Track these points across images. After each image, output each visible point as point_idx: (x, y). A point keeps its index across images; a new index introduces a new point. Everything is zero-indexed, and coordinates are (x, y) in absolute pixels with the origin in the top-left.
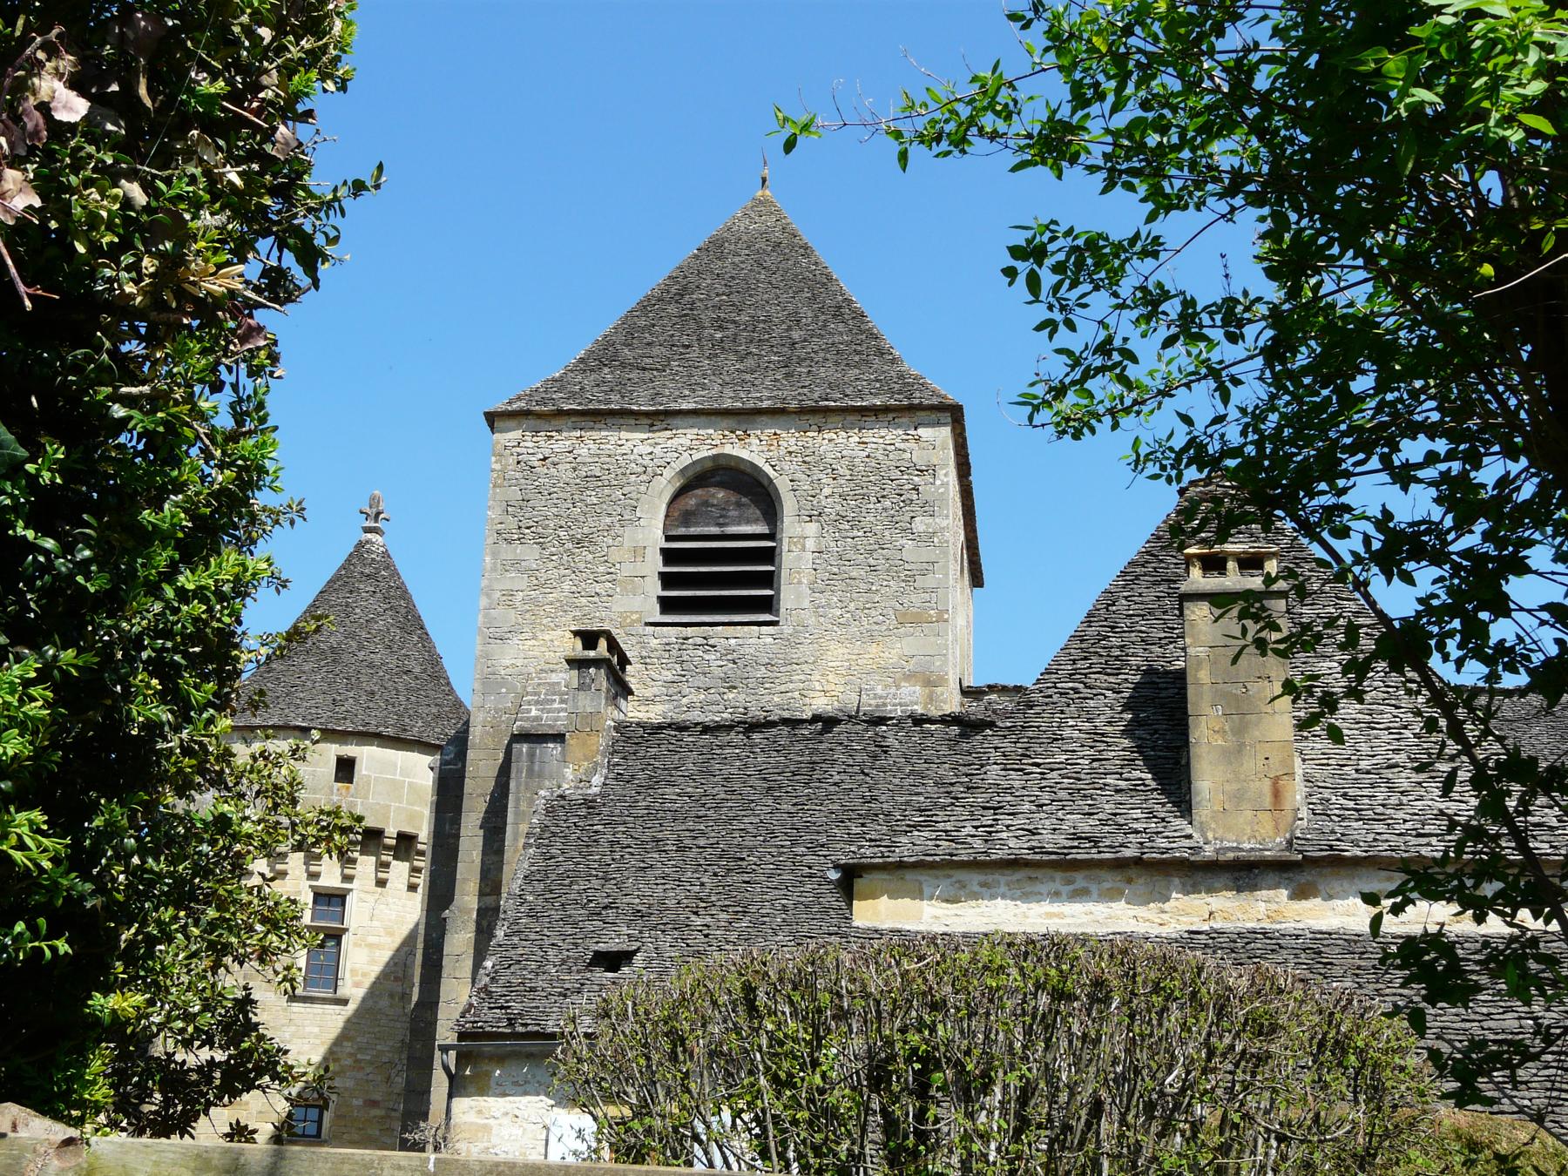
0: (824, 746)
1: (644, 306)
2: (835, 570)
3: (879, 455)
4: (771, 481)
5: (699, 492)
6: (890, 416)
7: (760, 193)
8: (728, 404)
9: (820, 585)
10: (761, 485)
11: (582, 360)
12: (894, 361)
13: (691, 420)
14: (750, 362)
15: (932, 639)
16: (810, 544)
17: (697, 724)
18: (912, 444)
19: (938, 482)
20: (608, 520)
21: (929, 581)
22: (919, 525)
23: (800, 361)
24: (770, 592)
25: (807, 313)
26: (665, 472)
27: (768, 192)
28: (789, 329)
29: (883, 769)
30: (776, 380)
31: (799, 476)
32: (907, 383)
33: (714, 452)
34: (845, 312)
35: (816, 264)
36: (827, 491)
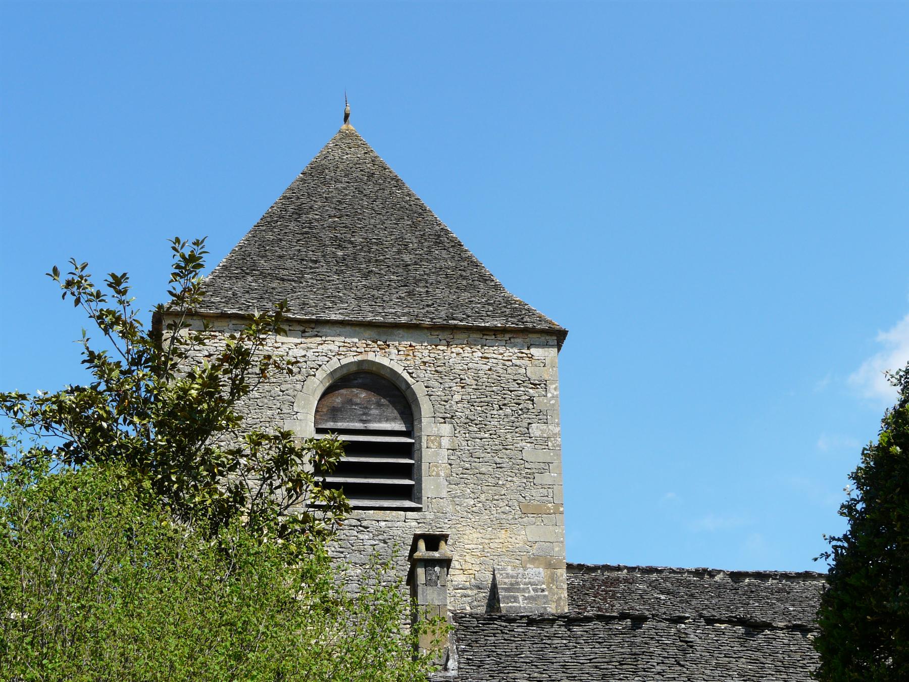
0: (638, 640)
1: (268, 221)
2: (468, 466)
3: (499, 368)
4: (408, 386)
5: (343, 391)
6: (507, 336)
7: (344, 127)
8: (370, 318)
9: (455, 478)
10: (398, 388)
11: (225, 268)
12: (497, 287)
13: (338, 330)
14: (374, 280)
15: (551, 528)
16: (445, 442)
17: (522, 617)
18: (526, 362)
19: (549, 395)
20: (269, 413)
21: (546, 479)
22: (536, 430)
23: (417, 282)
24: (412, 483)
25: (412, 240)
26: (318, 373)
27: (351, 127)
28: (399, 252)
29: (693, 661)
30: (400, 298)
31: (433, 383)
32: (518, 310)
33: (360, 358)
34: (441, 238)
35: (409, 195)
36: (457, 397)
